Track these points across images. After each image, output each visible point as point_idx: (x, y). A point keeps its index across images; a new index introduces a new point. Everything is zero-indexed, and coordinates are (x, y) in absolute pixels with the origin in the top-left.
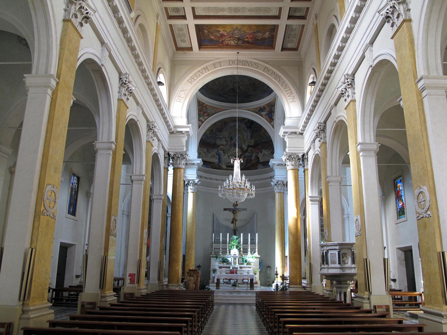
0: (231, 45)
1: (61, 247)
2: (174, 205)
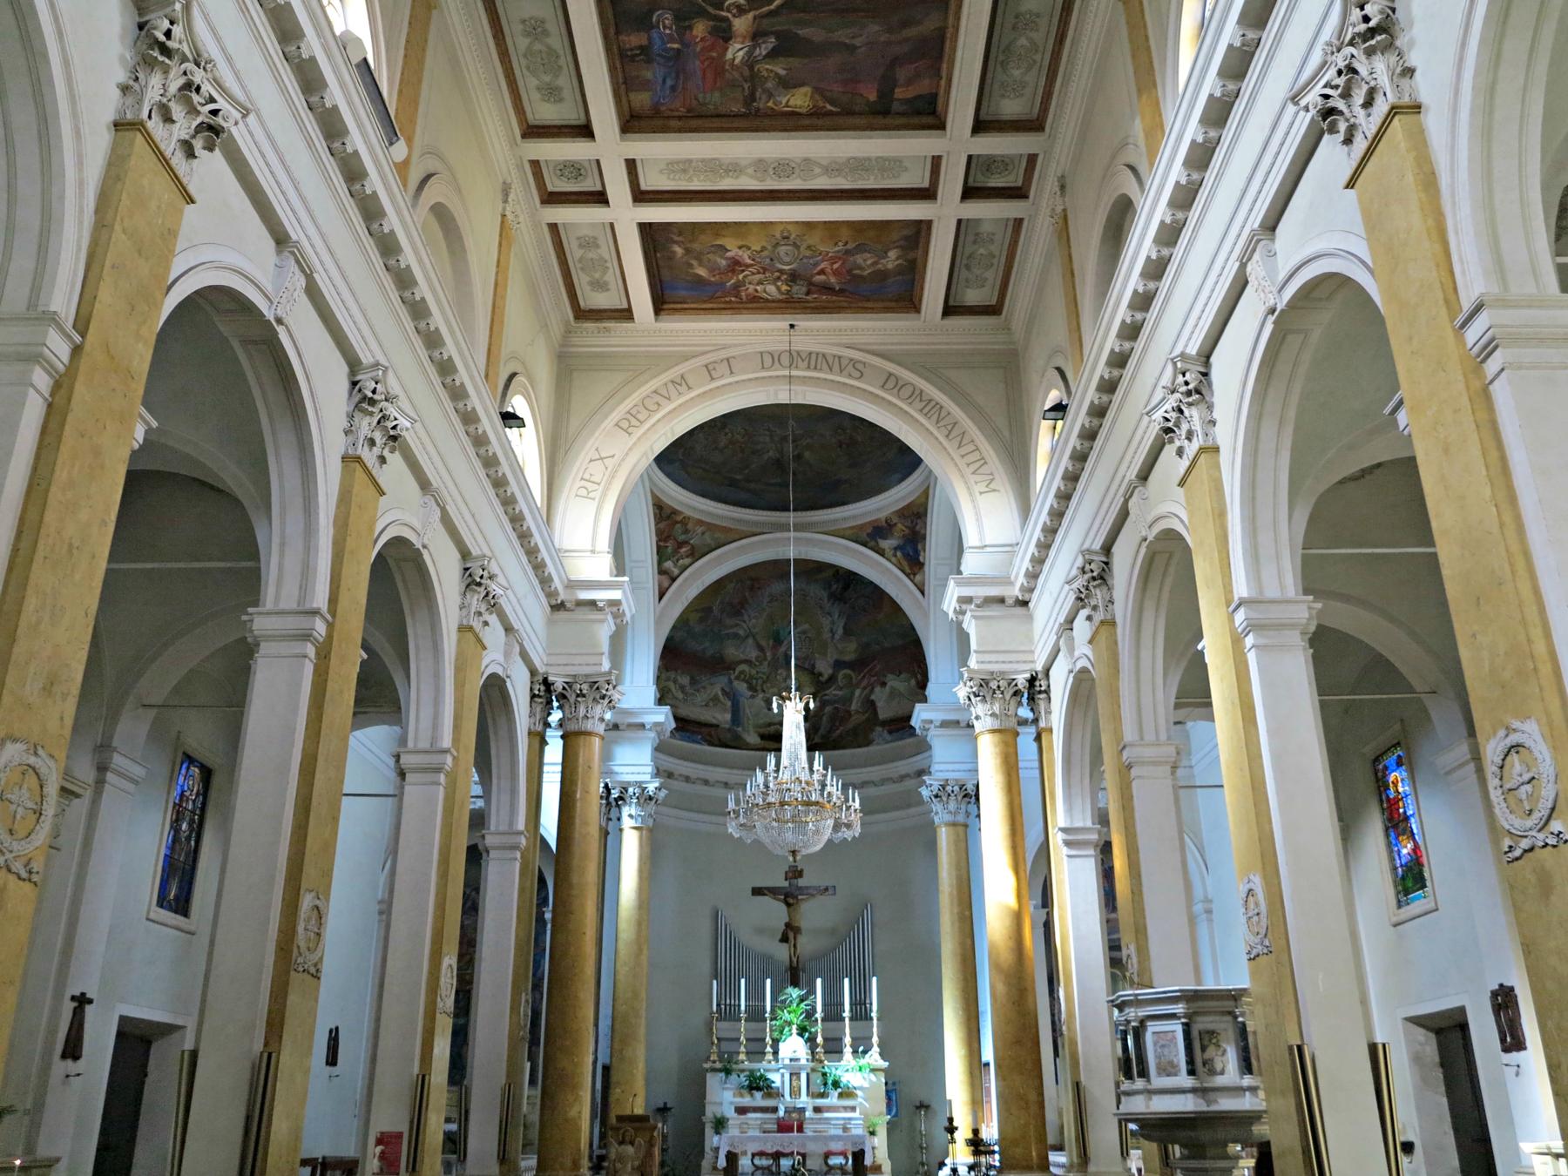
0: (767, 301)
1: (121, 1035)
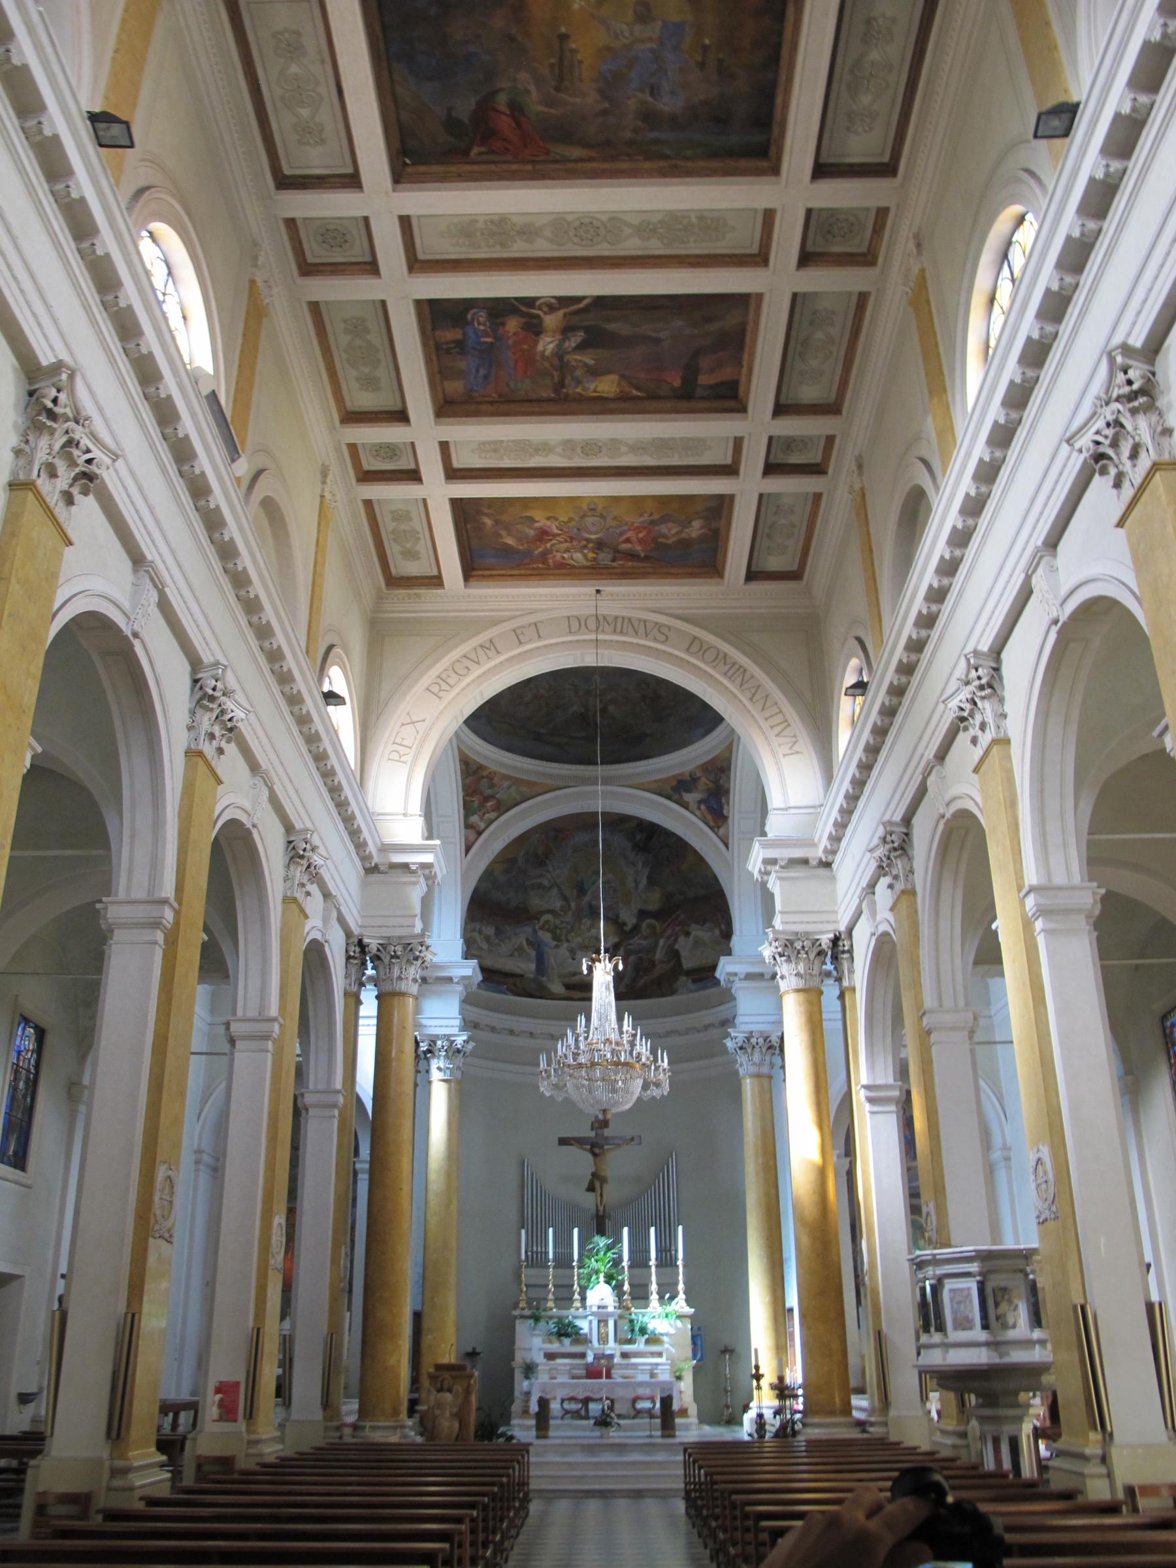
0: (573, 567)
2: (381, 1129)
